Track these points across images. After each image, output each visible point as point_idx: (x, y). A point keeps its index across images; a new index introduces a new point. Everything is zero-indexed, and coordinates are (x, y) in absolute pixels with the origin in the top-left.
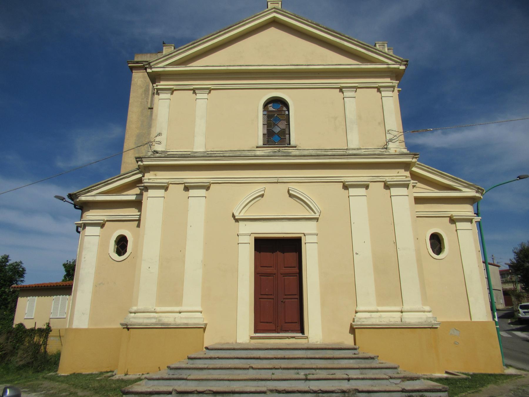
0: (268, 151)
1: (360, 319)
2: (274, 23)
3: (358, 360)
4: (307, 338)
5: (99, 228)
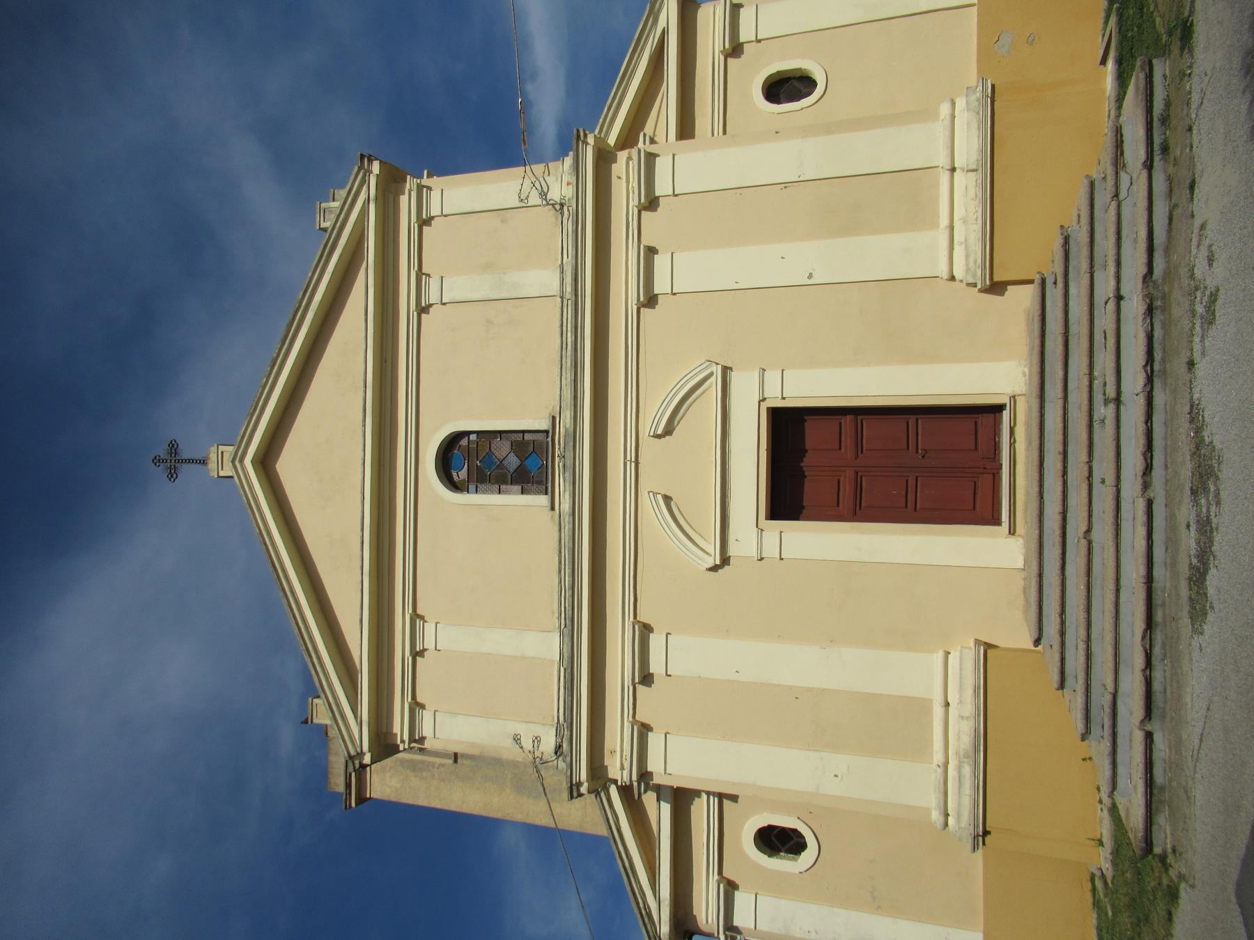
0: (561, 483)
1: (968, 270)
2: (266, 462)
3: (1071, 275)
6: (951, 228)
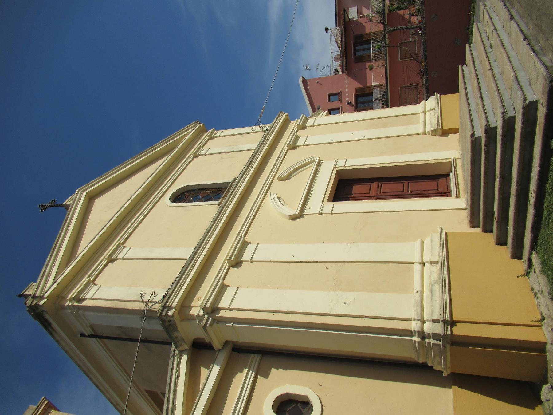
4: (455, 160)
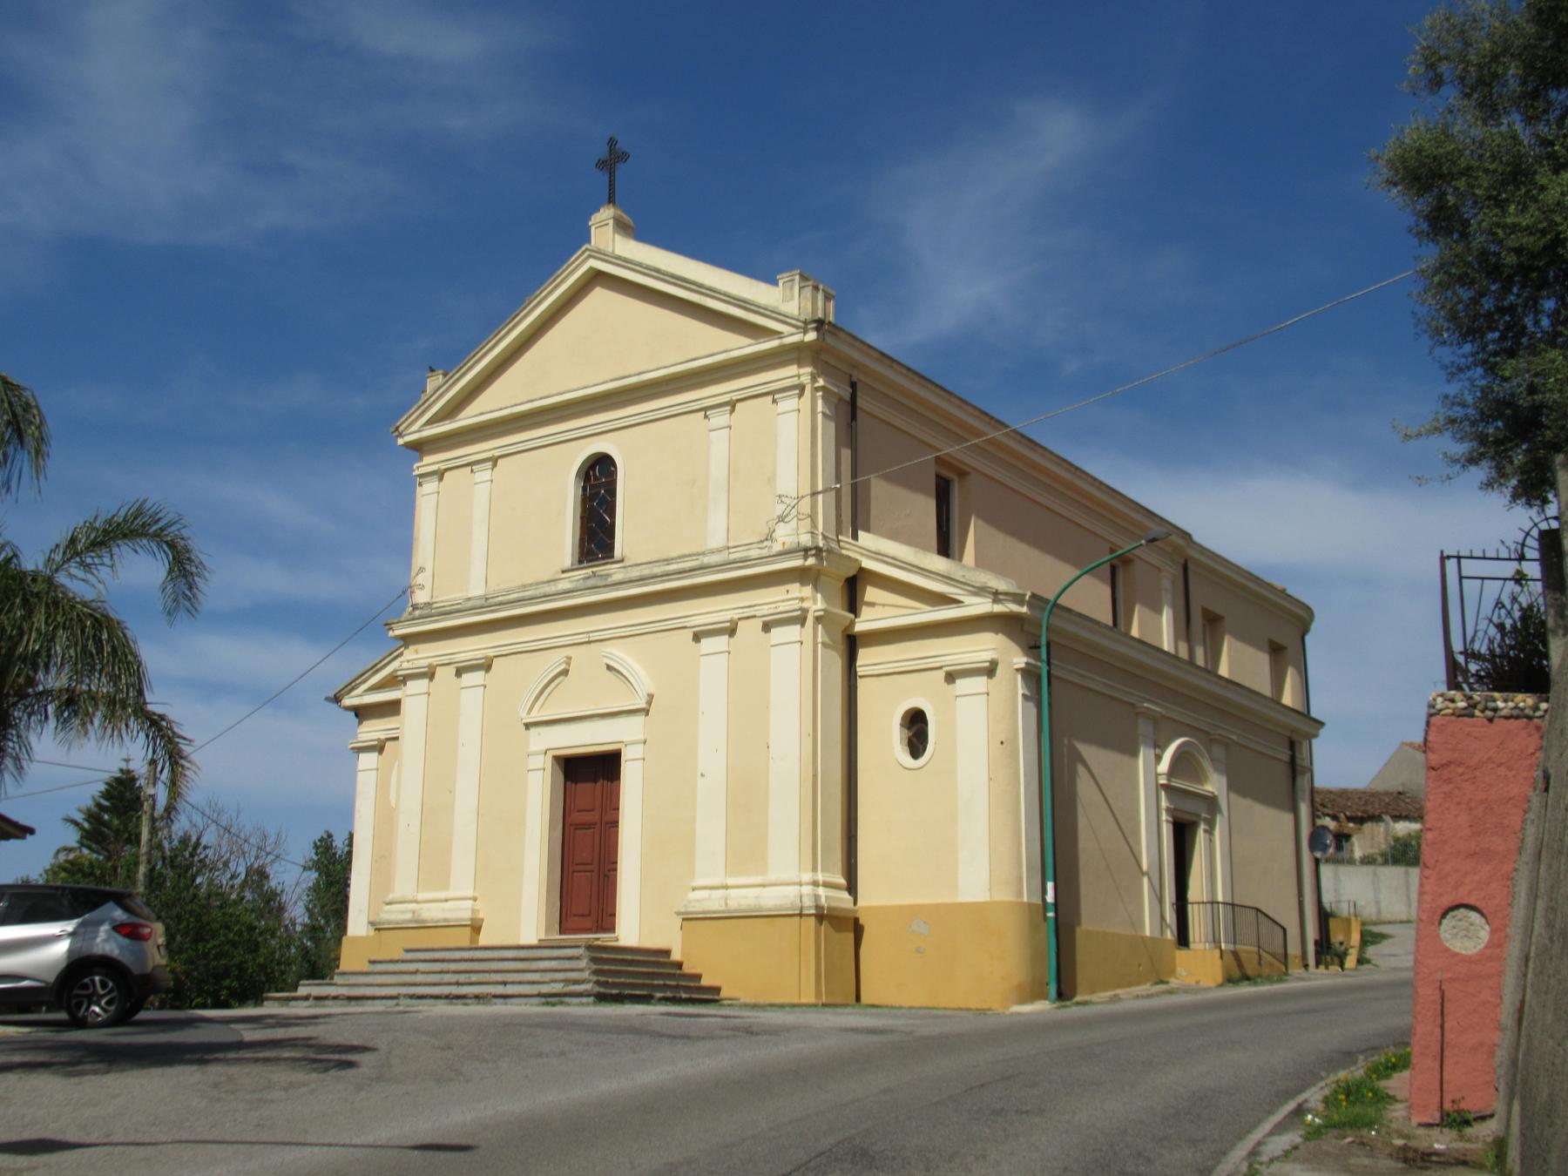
2: (597, 278)
5: (375, 755)
6: (726, 887)
